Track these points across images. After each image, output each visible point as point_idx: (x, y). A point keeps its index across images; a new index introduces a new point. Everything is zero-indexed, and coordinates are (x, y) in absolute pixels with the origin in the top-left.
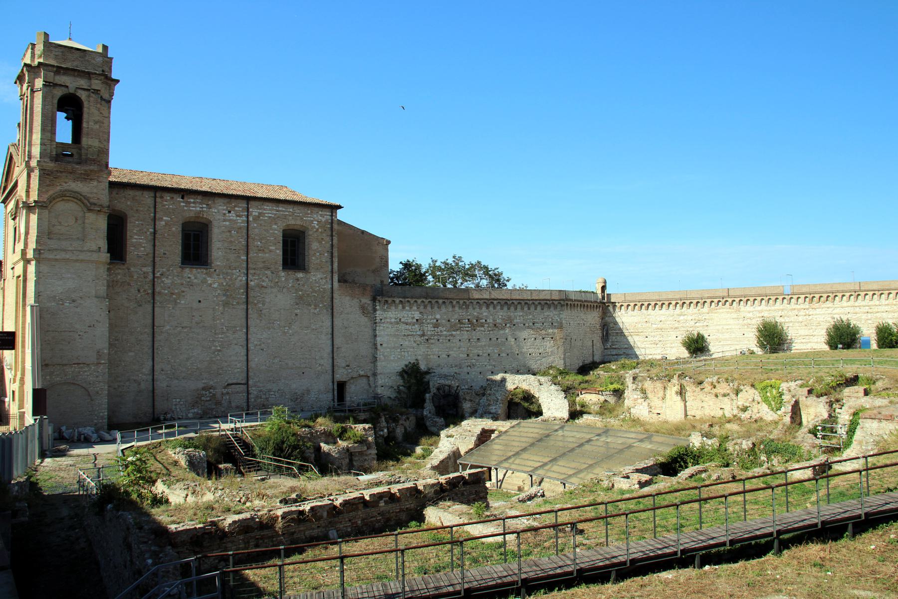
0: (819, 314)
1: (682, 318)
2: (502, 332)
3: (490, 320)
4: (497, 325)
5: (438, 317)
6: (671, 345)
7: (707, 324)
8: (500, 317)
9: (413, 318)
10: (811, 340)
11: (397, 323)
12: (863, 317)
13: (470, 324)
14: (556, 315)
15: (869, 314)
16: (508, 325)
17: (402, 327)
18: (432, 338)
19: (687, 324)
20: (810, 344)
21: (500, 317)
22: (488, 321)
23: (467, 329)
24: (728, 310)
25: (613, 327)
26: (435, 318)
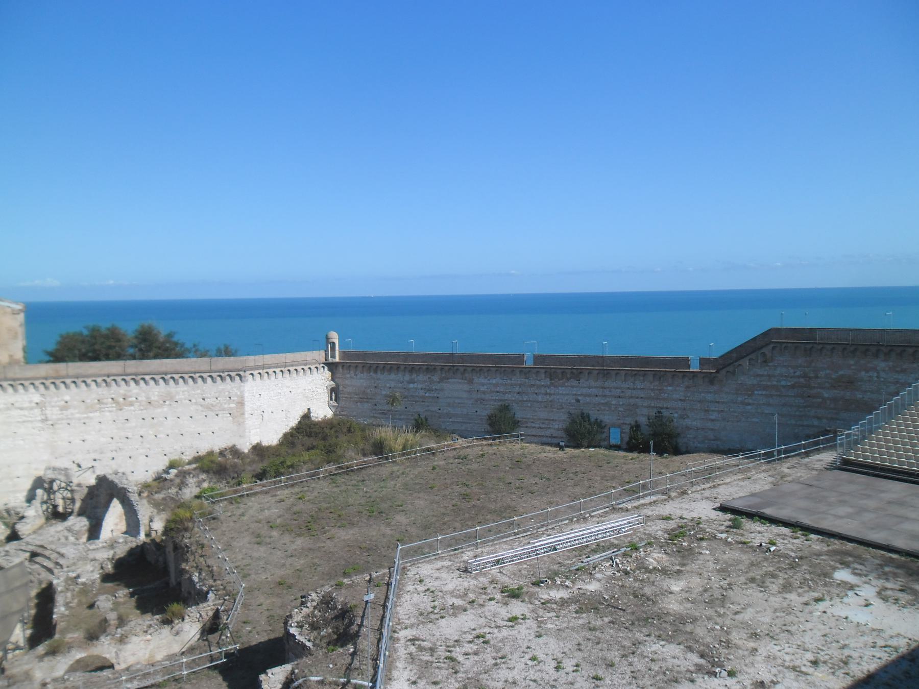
0: (562, 394)
1: (411, 386)
2: (159, 410)
3: (142, 398)
4: (152, 403)
5: (67, 398)
6: (400, 417)
7: (438, 395)
8: (156, 393)
9: (31, 402)
10: (551, 426)
11: (8, 409)
12: (613, 402)
13: (114, 403)
14: (235, 387)
15: (621, 399)
16: (167, 403)
17: (15, 413)
18: (59, 422)
19: (417, 394)
20: (549, 430)
21: (156, 393)
22: (140, 399)
23: (110, 409)
24: (460, 381)
25: (343, 391)
26: (63, 400)
